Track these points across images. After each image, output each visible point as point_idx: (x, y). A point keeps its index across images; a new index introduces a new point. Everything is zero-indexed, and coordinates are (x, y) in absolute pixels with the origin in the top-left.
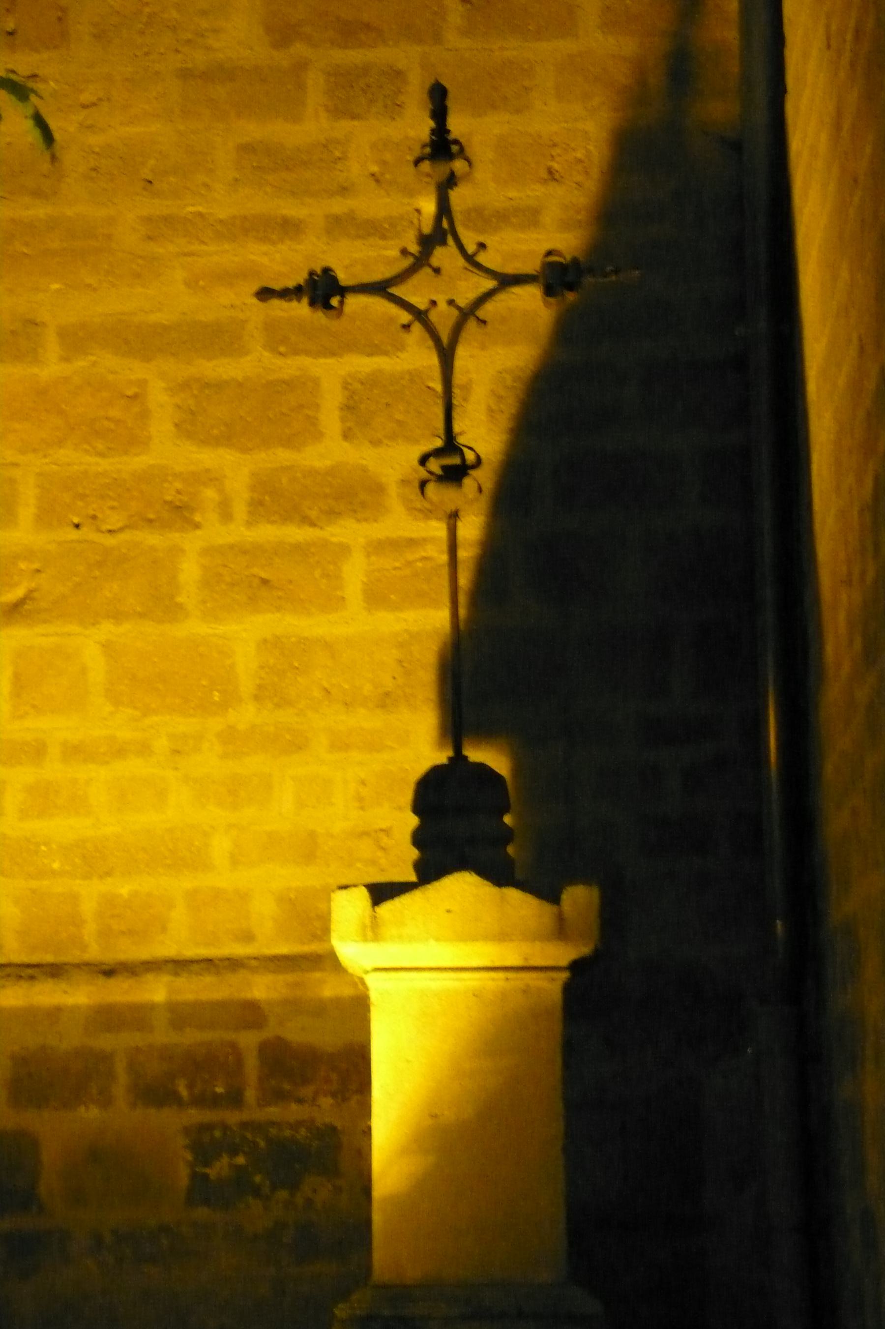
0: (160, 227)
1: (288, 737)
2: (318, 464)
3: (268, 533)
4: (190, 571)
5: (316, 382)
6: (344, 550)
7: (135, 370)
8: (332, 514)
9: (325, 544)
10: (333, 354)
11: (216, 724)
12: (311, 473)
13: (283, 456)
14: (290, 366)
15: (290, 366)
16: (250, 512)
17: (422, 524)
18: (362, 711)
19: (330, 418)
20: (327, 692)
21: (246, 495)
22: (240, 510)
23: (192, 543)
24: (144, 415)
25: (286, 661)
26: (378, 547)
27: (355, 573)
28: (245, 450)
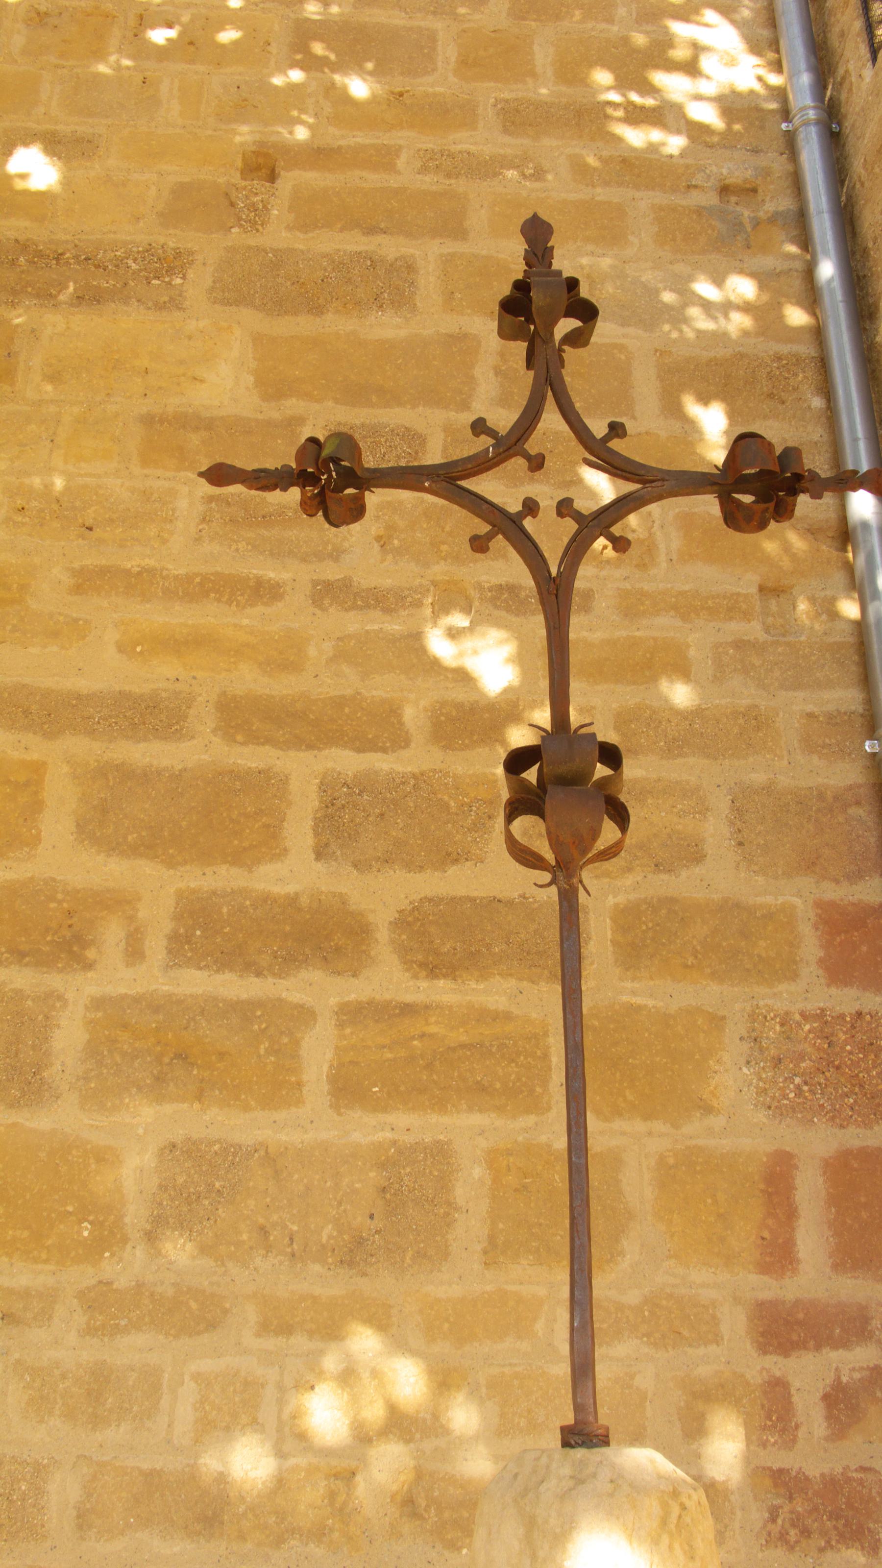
0: (87, 582)
1: (194, 1305)
2: (277, 889)
3: (196, 982)
4: (69, 1036)
5: (285, 781)
6: (305, 1015)
7: (35, 748)
8: (288, 963)
9: (275, 1007)
10: (310, 747)
11: (83, 1276)
12: (266, 899)
13: (223, 878)
14: (250, 758)
15: (250, 758)
16: (170, 951)
17: (424, 984)
18: (316, 1268)
19: (299, 832)
20: (263, 1231)
21: (168, 926)
22: (156, 946)
23: (79, 989)
24: (37, 806)
25: (198, 1186)
26: (352, 1014)
27: (318, 1052)
28: (171, 864)
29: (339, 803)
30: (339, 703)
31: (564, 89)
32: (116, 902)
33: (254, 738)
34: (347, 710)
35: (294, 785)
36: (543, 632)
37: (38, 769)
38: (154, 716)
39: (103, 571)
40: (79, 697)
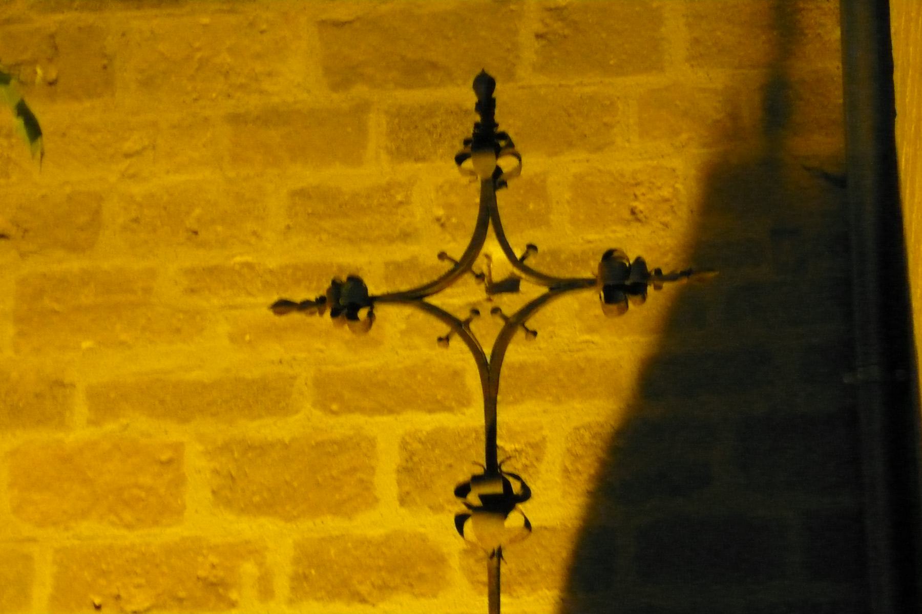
5: (372, 442)
10: (391, 411)
12: (363, 542)
13: (332, 525)
14: (342, 425)
15: (342, 425)
19: (386, 483)
21: (289, 569)
22: (282, 585)
24: (179, 482)
28: (289, 519)
29: (416, 459)
30: (411, 372)
31: (372, 145)
32: (251, 550)
33: (348, 408)
34: (419, 377)
35: (381, 445)
36: (507, 354)
37: (178, 448)
38: (267, 396)
39: (212, 271)
40: (204, 386)
